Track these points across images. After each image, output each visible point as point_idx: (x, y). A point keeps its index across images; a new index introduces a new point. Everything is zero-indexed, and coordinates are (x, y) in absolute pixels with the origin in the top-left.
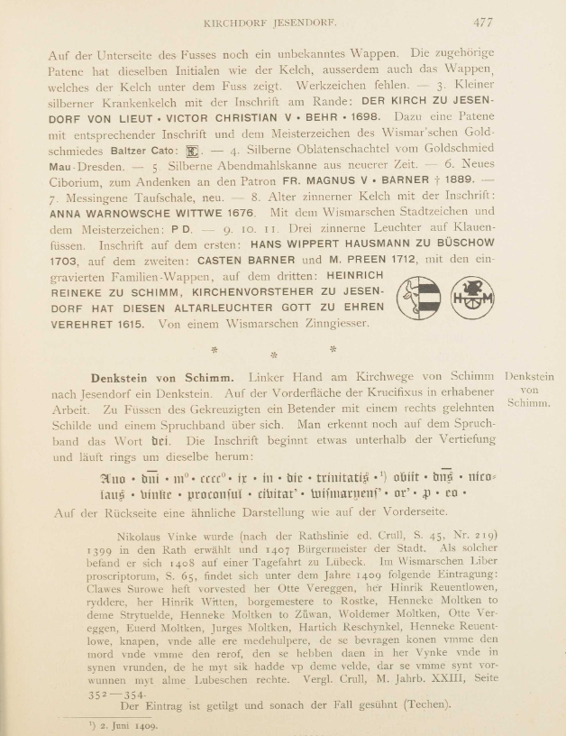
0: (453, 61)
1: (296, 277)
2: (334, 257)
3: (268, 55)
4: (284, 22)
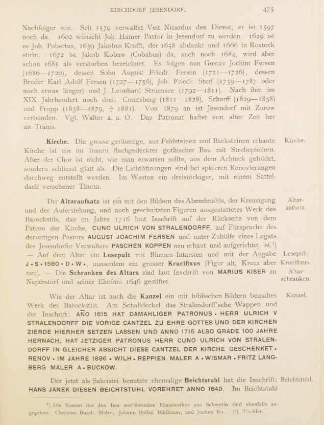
2: (220, 271)
3: (172, 297)
4: (156, 10)
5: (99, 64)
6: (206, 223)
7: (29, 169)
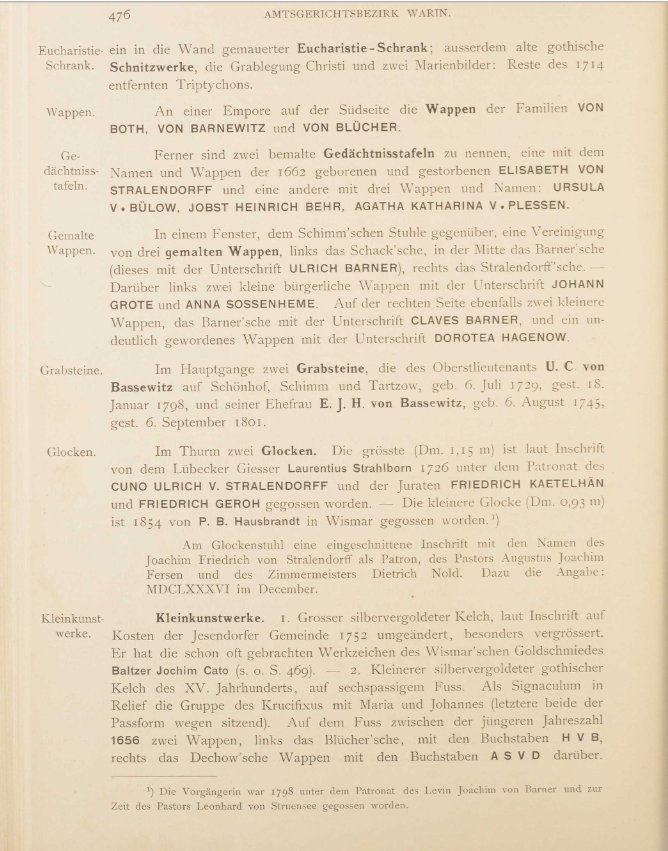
0: (196, 733)
1: (494, 251)
5: (460, 172)
6: (387, 119)
7: (487, 635)
